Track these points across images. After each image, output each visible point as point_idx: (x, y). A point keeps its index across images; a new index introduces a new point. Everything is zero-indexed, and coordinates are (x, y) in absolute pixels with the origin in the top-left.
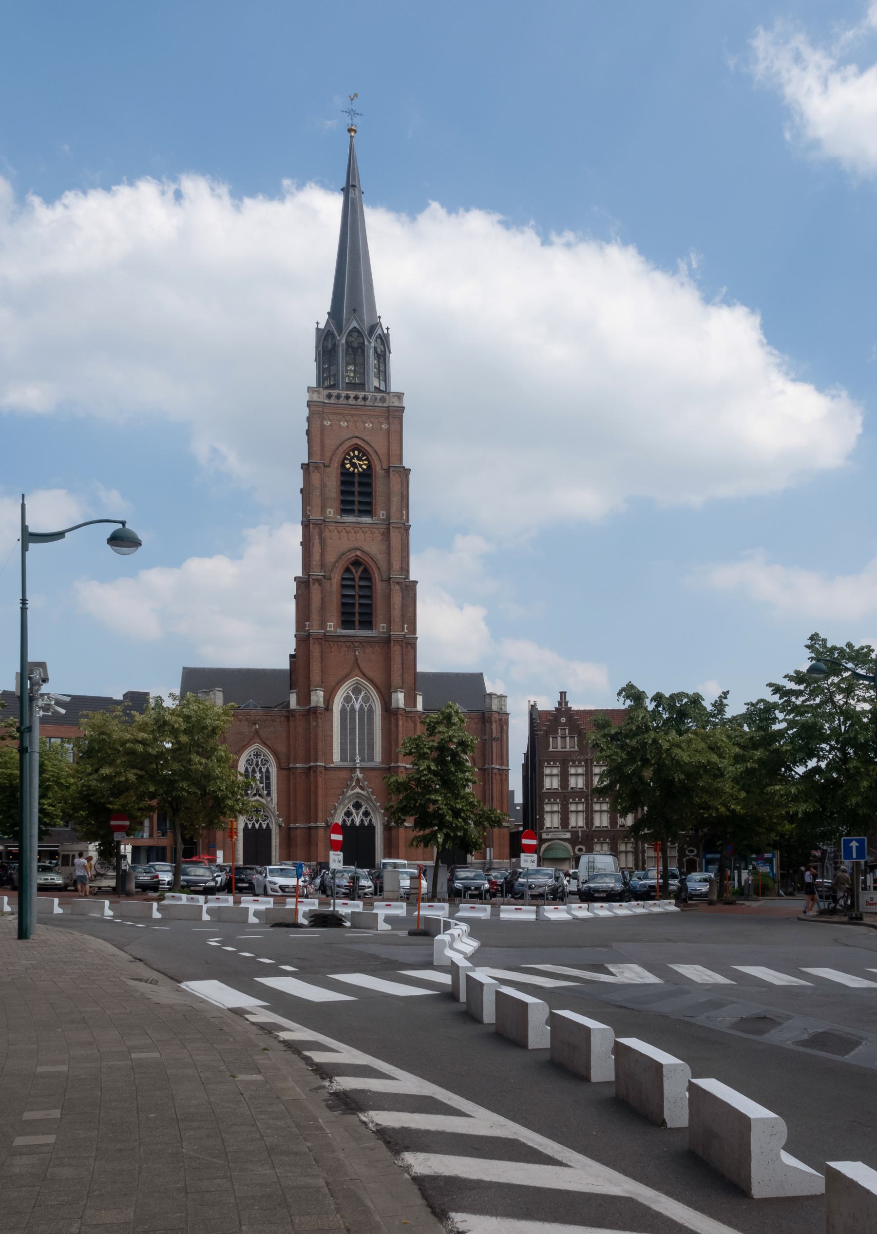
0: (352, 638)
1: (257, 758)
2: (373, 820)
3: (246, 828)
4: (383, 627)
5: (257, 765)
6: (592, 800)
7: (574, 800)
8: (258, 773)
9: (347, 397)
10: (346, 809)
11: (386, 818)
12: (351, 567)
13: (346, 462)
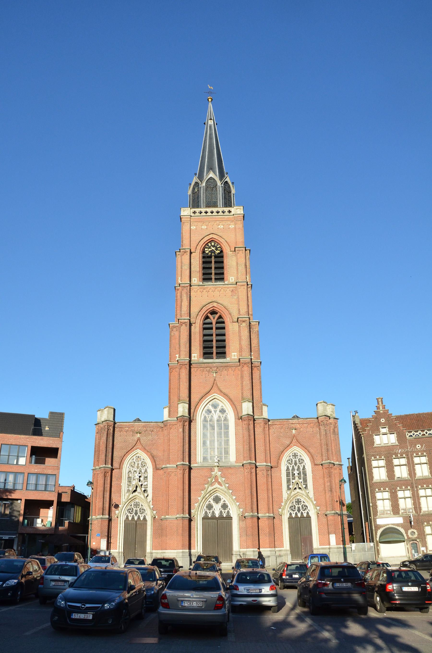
0: (210, 364)
1: (295, 458)
2: (231, 512)
3: (290, 518)
4: (234, 355)
5: (296, 464)
6: (417, 487)
7: (401, 488)
8: (296, 470)
9: (206, 212)
10: (207, 503)
11: (241, 510)
12: (209, 315)
13: (206, 249)
